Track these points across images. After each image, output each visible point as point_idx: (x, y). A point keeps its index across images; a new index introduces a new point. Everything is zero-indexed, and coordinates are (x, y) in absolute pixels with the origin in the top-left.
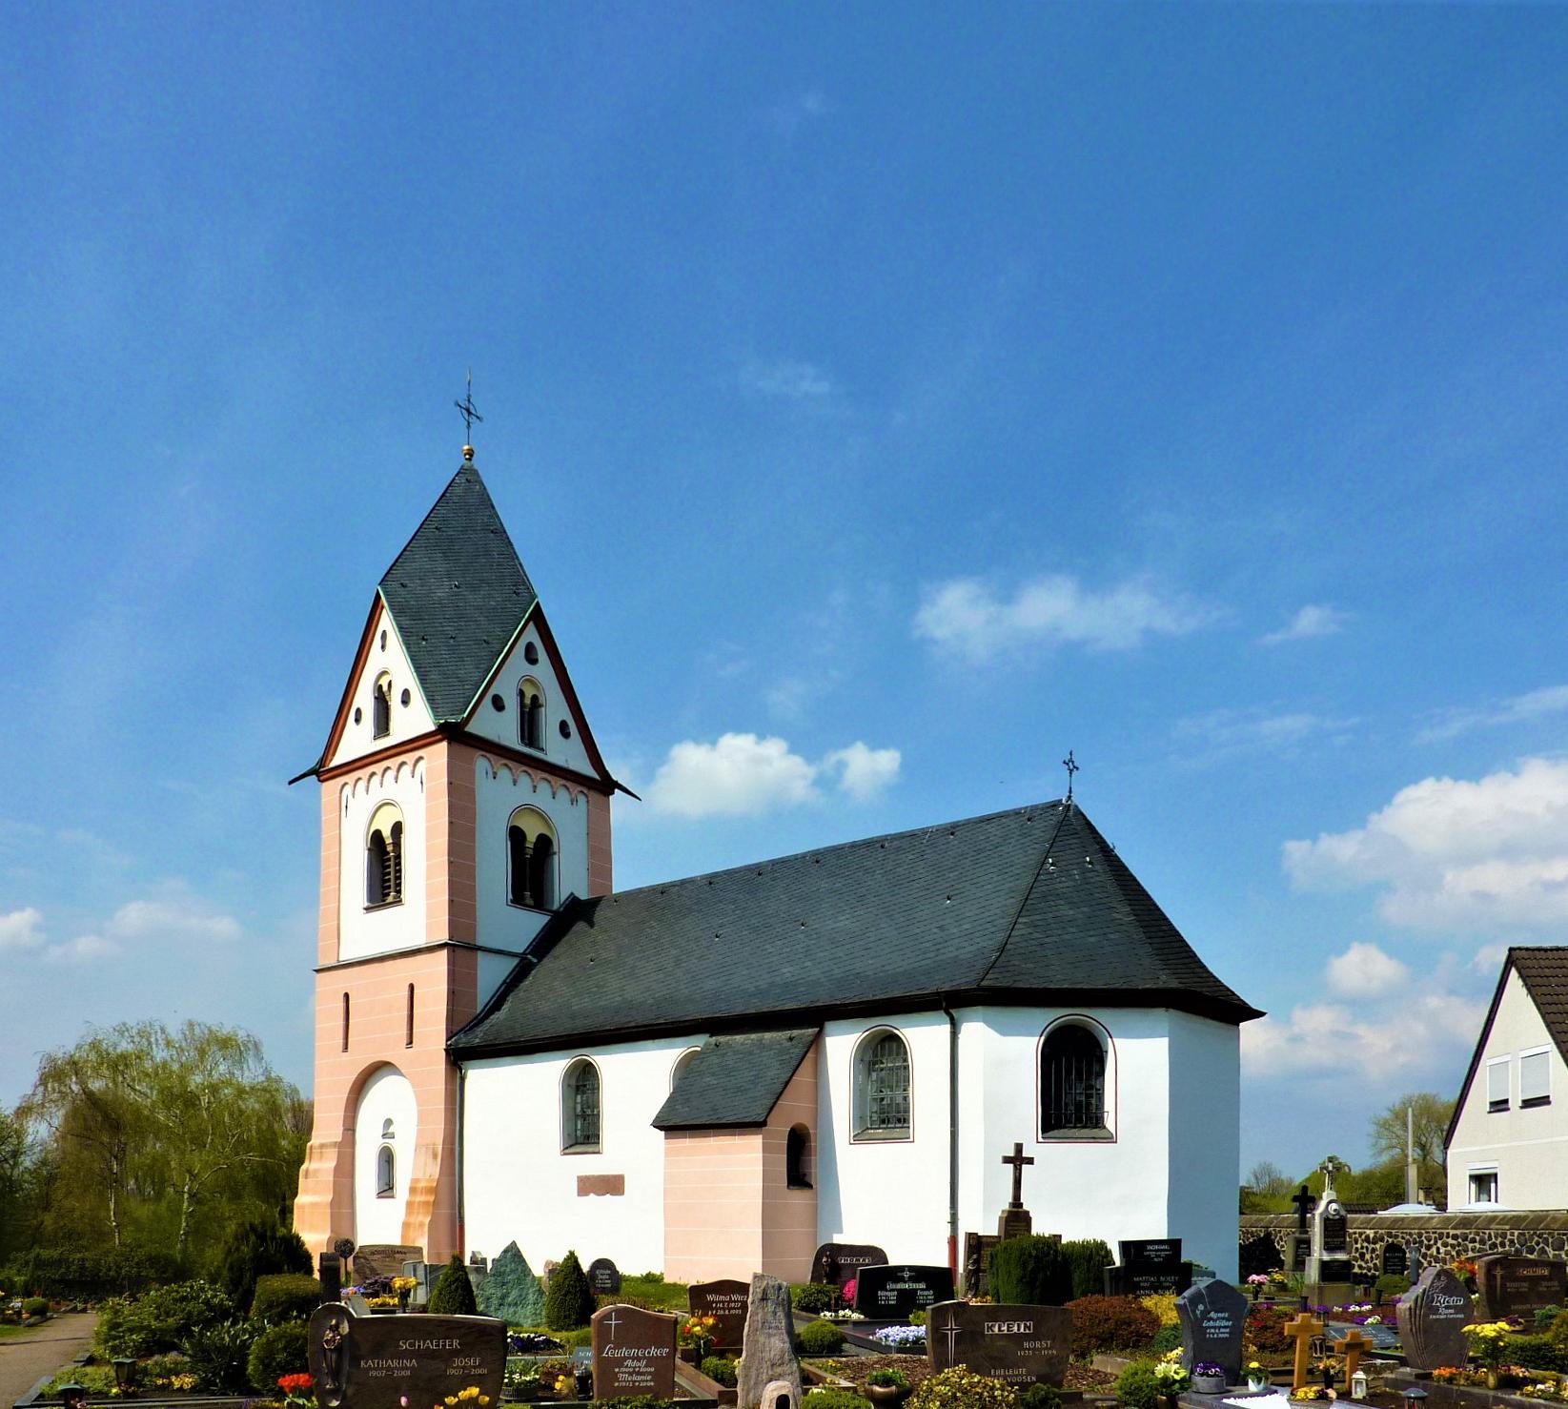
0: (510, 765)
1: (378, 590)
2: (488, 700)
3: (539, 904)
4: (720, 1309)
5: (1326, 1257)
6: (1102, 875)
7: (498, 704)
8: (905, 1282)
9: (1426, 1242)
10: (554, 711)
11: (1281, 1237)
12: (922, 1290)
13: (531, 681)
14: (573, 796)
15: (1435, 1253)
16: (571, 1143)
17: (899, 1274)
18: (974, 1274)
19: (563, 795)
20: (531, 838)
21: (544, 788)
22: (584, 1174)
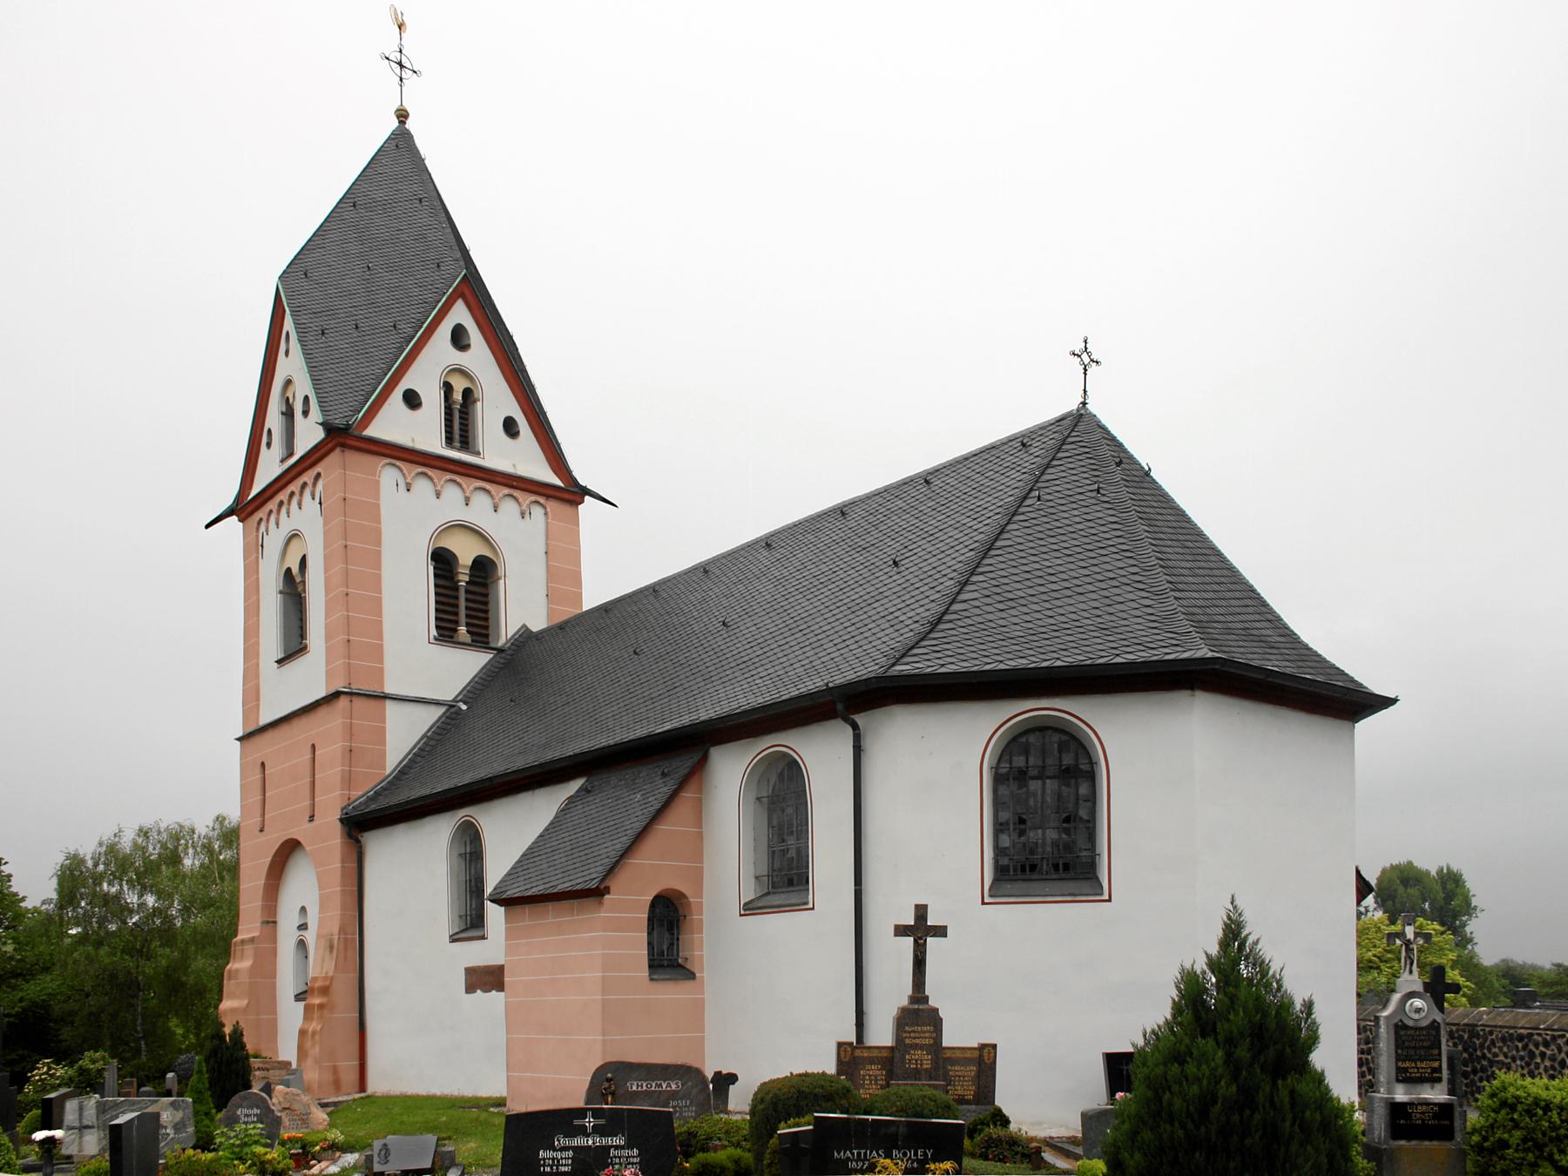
0: (430, 473)
3: (481, 637)
5: (1401, 1095)
6: (433, 188)
7: (412, 400)
8: (588, 1136)
10: (496, 403)
11: (1493, 1041)
12: (616, 1147)
14: (524, 507)
16: (462, 928)
17: (576, 1122)
19: (509, 508)
21: (481, 502)
22: (470, 965)
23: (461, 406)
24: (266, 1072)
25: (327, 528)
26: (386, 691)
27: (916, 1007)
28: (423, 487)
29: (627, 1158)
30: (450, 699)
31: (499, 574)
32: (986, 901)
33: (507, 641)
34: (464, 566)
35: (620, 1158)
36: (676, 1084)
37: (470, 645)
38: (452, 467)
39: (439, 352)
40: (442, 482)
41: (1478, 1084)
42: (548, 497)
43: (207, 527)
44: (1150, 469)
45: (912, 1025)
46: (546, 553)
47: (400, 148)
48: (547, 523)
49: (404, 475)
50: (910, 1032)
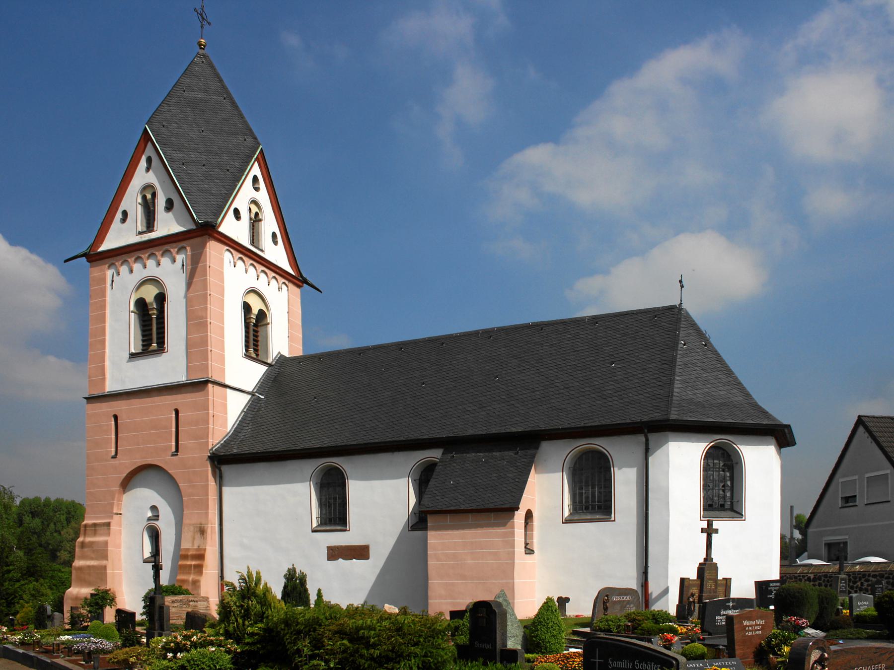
1: (146, 127)
2: (119, 216)
4: (750, 631)
7: (237, 213)
9: (853, 579)
13: (254, 202)
15: (860, 586)
20: (255, 311)
24: (196, 603)
33: (273, 360)
34: (254, 314)
38: (254, 257)
41: (206, 635)
42: (290, 281)
46: (288, 312)
48: (288, 295)
49: (233, 257)
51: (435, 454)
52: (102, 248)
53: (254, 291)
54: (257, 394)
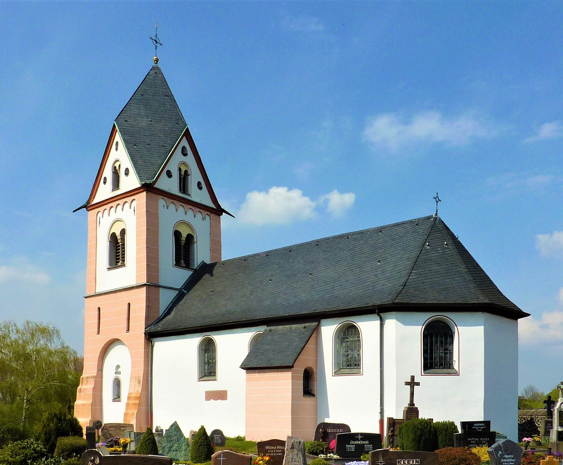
1: (114, 123)
3: (188, 266)
7: (169, 175)
8: (359, 441)
10: (195, 177)
12: (366, 444)
13: (184, 164)
18: (392, 437)
19: (199, 216)
20: (184, 235)
23: (184, 177)
25: (137, 221)
26: (160, 284)
27: (411, 407)
28: (172, 207)
29: (369, 447)
30: (179, 288)
31: (195, 241)
32: (422, 374)
35: (367, 447)
36: (341, 430)
37: (184, 267)
39: (178, 157)
40: (169, 202)
42: (211, 212)
43: (74, 212)
44: (458, 237)
45: (410, 413)
47: (156, 71)
50: (410, 415)
51: (262, 329)
52: (95, 201)
53: (183, 222)
54: (183, 290)
